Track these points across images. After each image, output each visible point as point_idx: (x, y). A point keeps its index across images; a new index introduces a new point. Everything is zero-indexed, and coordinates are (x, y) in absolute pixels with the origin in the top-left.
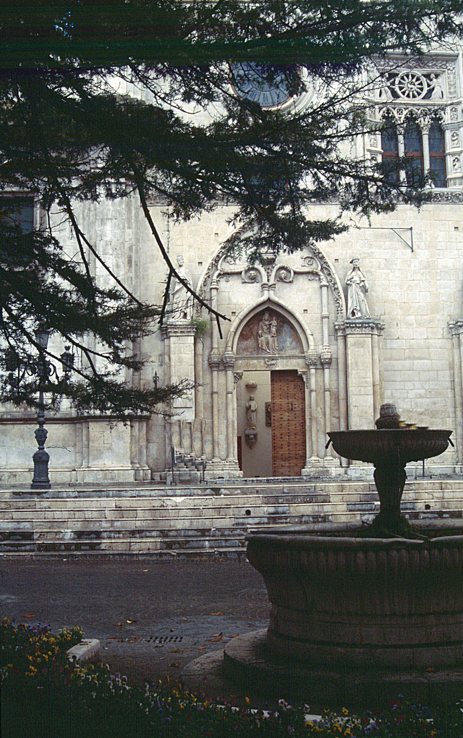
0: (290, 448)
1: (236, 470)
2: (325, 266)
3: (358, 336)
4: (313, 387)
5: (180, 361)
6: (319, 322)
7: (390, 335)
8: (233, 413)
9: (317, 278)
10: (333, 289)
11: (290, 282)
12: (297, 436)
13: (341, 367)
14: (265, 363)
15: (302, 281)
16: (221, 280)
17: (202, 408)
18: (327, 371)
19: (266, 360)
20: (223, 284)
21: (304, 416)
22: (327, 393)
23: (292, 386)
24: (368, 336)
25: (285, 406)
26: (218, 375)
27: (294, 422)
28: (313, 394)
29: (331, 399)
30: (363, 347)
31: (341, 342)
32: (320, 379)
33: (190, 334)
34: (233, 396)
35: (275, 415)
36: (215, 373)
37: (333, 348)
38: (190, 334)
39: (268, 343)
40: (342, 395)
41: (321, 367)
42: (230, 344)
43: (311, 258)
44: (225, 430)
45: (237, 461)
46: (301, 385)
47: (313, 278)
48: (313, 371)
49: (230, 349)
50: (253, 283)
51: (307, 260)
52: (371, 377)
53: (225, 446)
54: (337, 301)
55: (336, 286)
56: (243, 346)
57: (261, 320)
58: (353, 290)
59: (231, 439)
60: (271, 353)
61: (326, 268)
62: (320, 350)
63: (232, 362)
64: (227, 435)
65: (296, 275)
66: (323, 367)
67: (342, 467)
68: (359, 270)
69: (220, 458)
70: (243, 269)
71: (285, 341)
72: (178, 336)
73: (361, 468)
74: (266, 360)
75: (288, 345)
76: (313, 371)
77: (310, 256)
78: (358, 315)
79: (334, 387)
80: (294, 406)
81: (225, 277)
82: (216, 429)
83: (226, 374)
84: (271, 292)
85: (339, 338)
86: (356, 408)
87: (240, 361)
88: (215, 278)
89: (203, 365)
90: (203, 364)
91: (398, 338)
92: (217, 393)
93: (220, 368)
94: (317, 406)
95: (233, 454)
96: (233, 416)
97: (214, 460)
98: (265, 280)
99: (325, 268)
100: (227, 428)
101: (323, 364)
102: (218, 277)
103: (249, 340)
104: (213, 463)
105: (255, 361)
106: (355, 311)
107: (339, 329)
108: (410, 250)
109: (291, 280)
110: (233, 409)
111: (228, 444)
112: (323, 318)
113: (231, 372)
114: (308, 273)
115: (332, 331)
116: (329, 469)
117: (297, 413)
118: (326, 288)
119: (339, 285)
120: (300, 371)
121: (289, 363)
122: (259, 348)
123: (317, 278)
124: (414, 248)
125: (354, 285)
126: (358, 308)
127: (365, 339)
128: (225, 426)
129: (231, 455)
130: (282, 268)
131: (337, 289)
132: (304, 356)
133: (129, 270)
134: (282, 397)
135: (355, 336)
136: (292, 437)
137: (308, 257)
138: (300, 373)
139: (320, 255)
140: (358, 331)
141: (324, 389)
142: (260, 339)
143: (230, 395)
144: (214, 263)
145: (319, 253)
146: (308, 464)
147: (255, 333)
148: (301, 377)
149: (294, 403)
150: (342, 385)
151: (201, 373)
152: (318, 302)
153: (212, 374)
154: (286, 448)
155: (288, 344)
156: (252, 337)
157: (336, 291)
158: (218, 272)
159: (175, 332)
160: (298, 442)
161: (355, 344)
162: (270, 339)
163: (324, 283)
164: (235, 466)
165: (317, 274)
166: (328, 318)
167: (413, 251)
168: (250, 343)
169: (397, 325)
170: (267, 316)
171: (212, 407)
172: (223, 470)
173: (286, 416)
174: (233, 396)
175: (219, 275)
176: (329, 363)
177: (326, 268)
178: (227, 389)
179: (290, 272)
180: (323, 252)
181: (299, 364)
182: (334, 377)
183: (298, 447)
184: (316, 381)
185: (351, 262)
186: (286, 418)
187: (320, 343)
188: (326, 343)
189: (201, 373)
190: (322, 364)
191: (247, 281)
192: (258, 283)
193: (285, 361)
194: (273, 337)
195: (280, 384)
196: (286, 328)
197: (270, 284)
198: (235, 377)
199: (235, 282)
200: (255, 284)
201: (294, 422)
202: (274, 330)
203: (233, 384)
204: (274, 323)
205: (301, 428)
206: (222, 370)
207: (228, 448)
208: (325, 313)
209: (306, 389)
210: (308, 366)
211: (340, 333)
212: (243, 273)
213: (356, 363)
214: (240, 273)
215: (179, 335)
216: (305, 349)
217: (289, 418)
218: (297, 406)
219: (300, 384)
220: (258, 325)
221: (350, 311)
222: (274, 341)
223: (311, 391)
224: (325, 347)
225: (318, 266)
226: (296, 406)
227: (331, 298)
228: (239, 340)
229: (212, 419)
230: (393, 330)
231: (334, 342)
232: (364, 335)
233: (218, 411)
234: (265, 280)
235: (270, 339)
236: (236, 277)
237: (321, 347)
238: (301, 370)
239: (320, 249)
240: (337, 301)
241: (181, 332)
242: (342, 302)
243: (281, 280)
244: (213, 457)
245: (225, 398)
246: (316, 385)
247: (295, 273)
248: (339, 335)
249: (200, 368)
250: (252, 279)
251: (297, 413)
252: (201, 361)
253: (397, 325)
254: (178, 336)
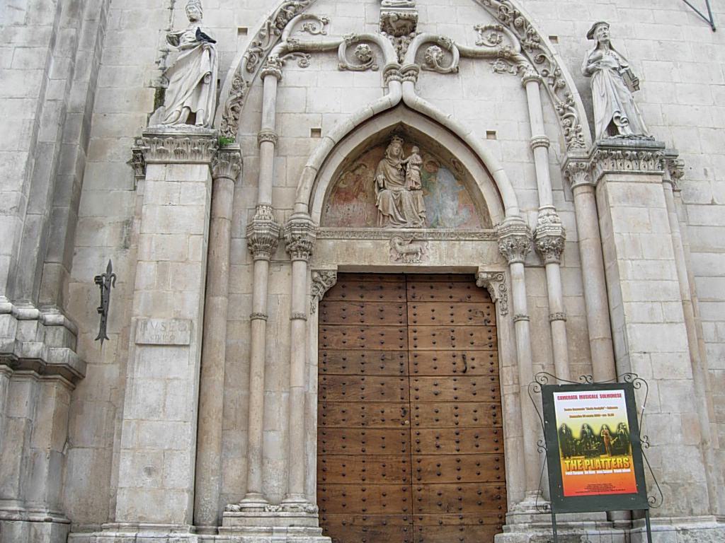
0: (461, 474)
1: (310, 533)
2: (529, 42)
3: (633, 178)
4: (521, 305)
5: (168, 224)
6: (525, 159)
7: (692, 194)
8: (307, 373)
9: (514, 69)
10: (552, 89)
11: (452, 72)
12: (479, 442)
13: (590, 258)
14: (393, 248)
15: (478, 73)
16: (290, 62)
17: (222, 357)
18: (553, 270)
19: (397, 241)
20: (293, 70)
21: (497, 389)
22: (558, 326)
23: (462, 310)
24: (653, 178)
25: (446, 365)
26: (270, 274)
27: (472, 406)
28: (523, 327)
29: (568, 344)
30: (645, 204)
31: (583, 201)
32: (537, 291)
33: (198, 159)
34: (307, 330)
35: (418, 384)
36: (262, 267)
37: (566, 219)
38: (198, 159)
39: (399, 204)
40: (598, 331)
41: (537, 263)
42: (304, 196)
43: (498, 30)
44: (283, 418)
45: (313, 507)
46: (486, 311)
47: (504, 67)
48: (518, 269)
49: (303, 208)
50: (365, 70)
51: (488, 34)
52: (675, 278)
53: (281, 464)
54: (564, 113)
55: (559, 81)
56: (339, 216)
57: (383, 157)
58: (604, 84)
59: (297, 445)
60: (409, 224)
61: (532, 48)
62: (533, 220)
63: (308, 239)
64: (288, 433)
65: (464, 62)
66: (542, 259)
67: (614, 526)
68: (611, 48)
69: (264, 496)
70: (342, 40)
71: (441, 208)
72: (166, 163)
73: (679, 526)
74: (397, 241)
75: (450, 216)
76: (518, 269)
77: (494, 25)
78: (625, 130)
79: (573, 309)
80: (470, 363)
81: (299, 59)
82: (256, 416)
83: (291, 274)
84: (408, 85)
85: (577, 191)
86: (647, 355)
87: (331, 243)
88: (274, 54)
89: (231, 248)
90: (231, 246)
91: (713, 203)
92: (265, 317)
93: (276, 258)
94: (534, 358)
95: (305, 485)
96: (307, 382)
97: (247, 503)
98: (392, 58)
99: (533, 46)
100: (289, 413)
101: (542, 252)
102: (281, 54)
103: (354, 202)
104: (241, 509)
105: (369, 244)
106: (617, 123)
107: (578, 170)
108: (709, 29)
109: (453, 66)
110: (307, 364)
111: (289, 459)
112: (533, 147)
113: (303, 265)
114: (491, 57)
115: (559, 176)
116: (579, 532)
117: (479, 380)
118: (535, 85)
119: (567, 77)
120: (485, 269)
121: (456, 250)
122: (379, 215)
123: (514, 69)
124: (716, 25)
125: (606, 71)
126: (623, 116)
127: (648, 185)
128: (283, 410)
129: (297, 487)
130: (432, 42)
131: (563, 87)
132: (495, 235)
133: (69, 23)
134: (435, 339)
135: (623, 178)
136: (467, 445)
137: (490, 28)
138: (484, 276)
139: (519, 20)
140: (628, 166)
141: (550, 315)
142: (379, 195)
143: (298, 324)
144: (273, 25)
145: (515, 15)
146: (516, 519)
147: (367, 187)
148: (485, 292)
149: (469, 355)
150: (595, 301)
151: (224, 265)
152: (521, 116)
153: (253, 272)
154: (449, 475)
155: (449, 213)
156: (361, 195)
157: (561, 93)
158: (283, 44)
159: (161, 152)
160: (481, 458)
161: (627, 197)
162: (406, 195)
163: (530, 72)
164: (306, 521)
165: (511, 59)
166: (547, 146)
167: (714, 30)
168: (357, 207)
169: (706, 173)
170: (396, 147)
171: (250, 357)
172: (270, 532)
173: (448, 388)
174: (307, 330)
175: (285, 52)
176: (559, 251)
177: (532, 48)
178: (291, 309)
179: (450, 52)
180: (523, 13)
181: (481, 255)
182: (573, 288)
183: (483, 472)
184: (528, 297)
185: (590, 35)
186: (448, 394)
187: (531, 205)
188: (546, 201)
189: (224, 265)
190: (540, 253)
191: (349, 65)
192: (376, 70)
193: (444, 245)
194: (412, 189)
195: (431, 306)
196: (444, 179)
197: (403, 67)
198: (315, 281)
199: (321, 69)
200: (370, 73)
201: (472, 406)
202: (414, 173)
203: (310, 298)
204: (415, 158)
205: (491, 421)
206: (280, 263)
207: (288, 470)
208: (538, 133)
209: (501, 318)
210: (504, 257)
211: (580, 179)
212: (342, 49)
213: (635, 243)
214: (333, 50)
215: (172, 159)
216: (495, 218)
217: (457, 393)
218: (479, 361)
219: (482, 307)
220: (376, 168)
221: (601, 128)
222: (415, 200)
223: (516, 319)
224: (545, 212)
225: (512, 43)
226: (474, 363)
227: (548, 108)
228: (326, 200)
229: (249, 388)
230: (694, 184)
231: (564, 205)
232: (645, 178)
233: (266, 366)
234: (392, 58)
235: (406, 195)
236: (323, 58)
237: (533, 214)
238: (487, 270)
239: (516, 5)
240: (564, 113)
241: (177, 152)
242: (579, 112)
243: (432, 66)
244: (247, 492)
245: (285, 334)
246: (529, 305)
247: (464, 55)
248: (578, 183)
249: (222, 250)
250: (363, 62)
251: (479, 380)
252: (227, 235)
253: (706, 173)
254: (166, 163)
